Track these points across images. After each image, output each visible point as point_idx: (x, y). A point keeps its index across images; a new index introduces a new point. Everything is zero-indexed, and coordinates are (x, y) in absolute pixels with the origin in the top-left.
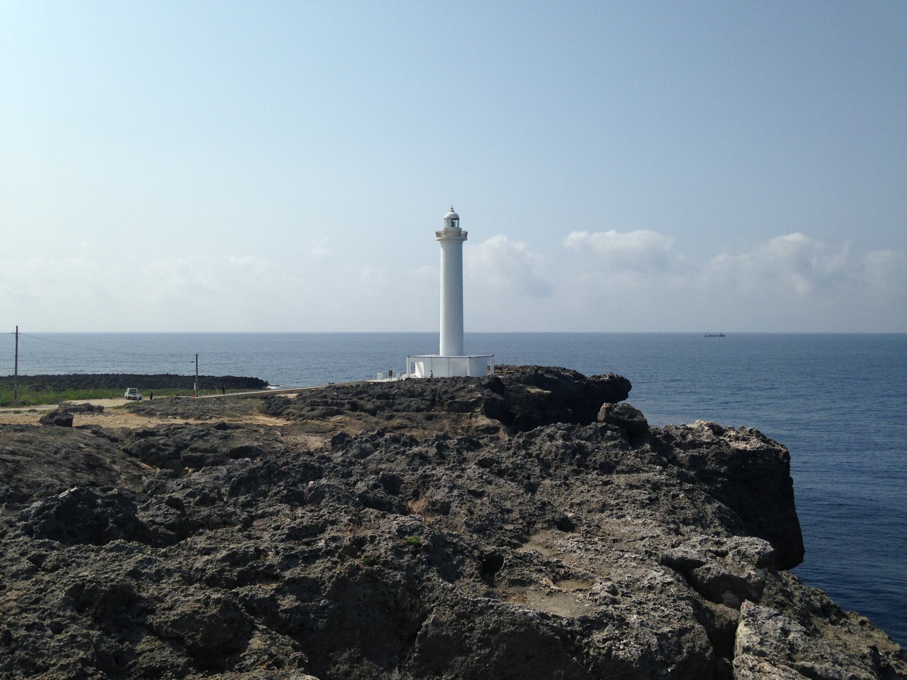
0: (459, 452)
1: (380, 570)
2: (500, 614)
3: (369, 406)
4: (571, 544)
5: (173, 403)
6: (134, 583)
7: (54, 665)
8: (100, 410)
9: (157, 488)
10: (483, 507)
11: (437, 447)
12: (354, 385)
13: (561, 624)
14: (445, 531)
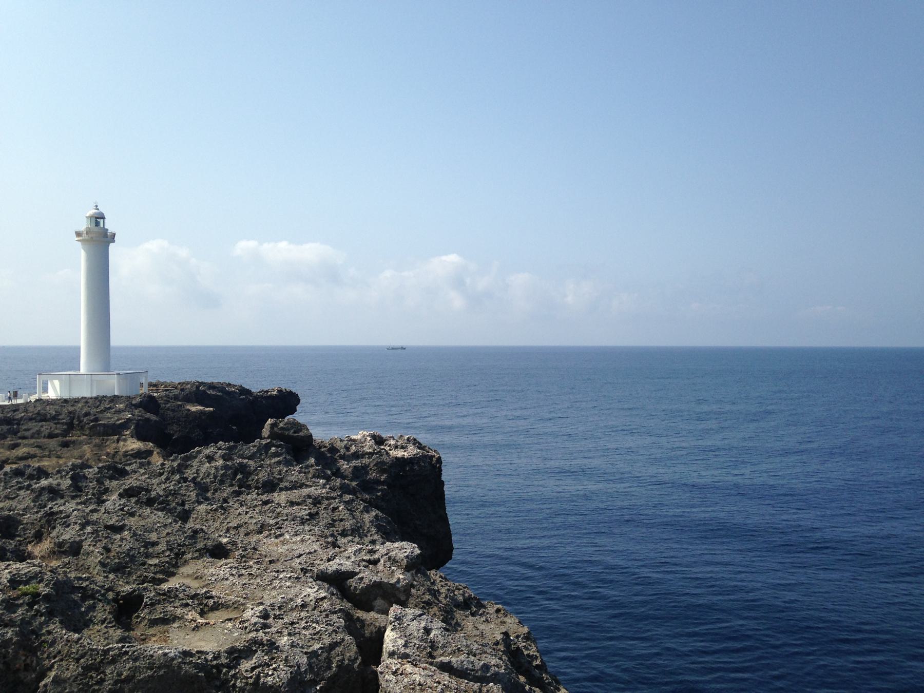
0: (100, 482)
4: (224, 572)
10: (123, 543)
11: (72, 478)
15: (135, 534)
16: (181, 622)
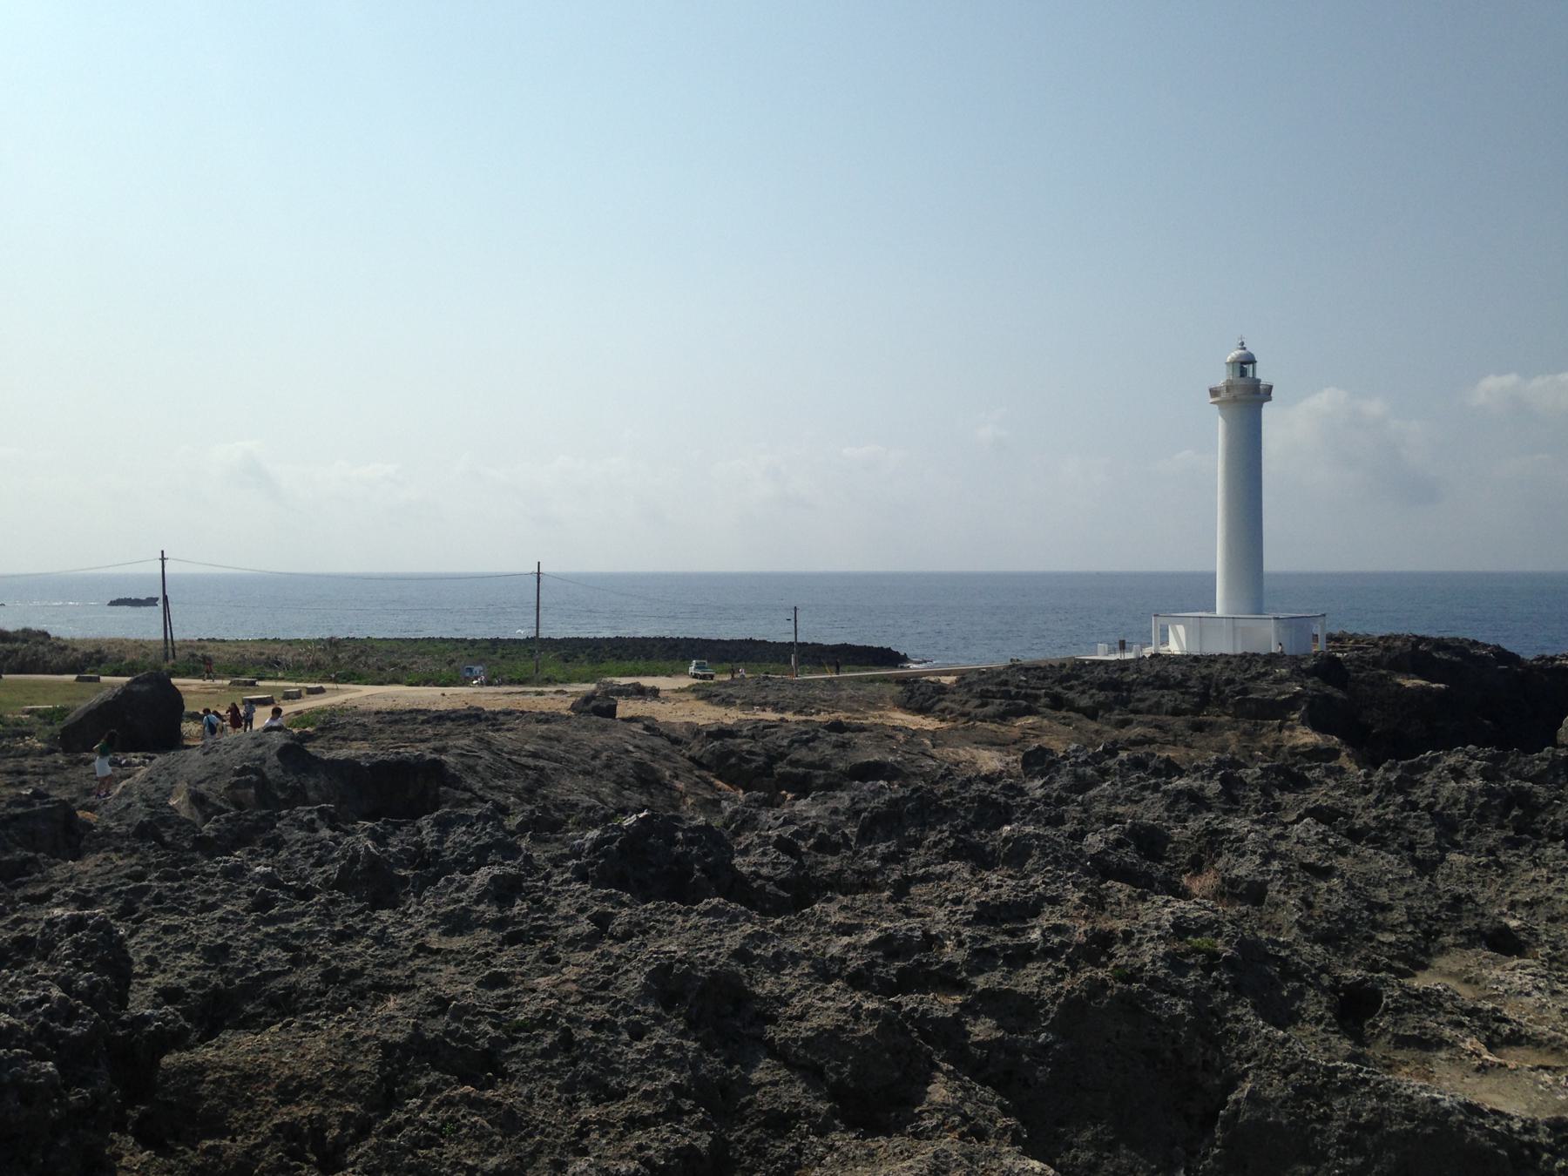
0: (1266, 792)
1: (1143, 994)
2: (1383, 1097)
3: (1084, 702)
4: (1520, 979)
5: (760, 686)
6: (742, 970)
7: (634, 1090)
8: (654, 693)
9: (744, 822)
10: (1332, 896)
11: (1223, 780)
12: (1056, 664)
13: (1510, 1129)
14: (1263, 935)
15: (1350, 886)
16: (1454, 1051)
